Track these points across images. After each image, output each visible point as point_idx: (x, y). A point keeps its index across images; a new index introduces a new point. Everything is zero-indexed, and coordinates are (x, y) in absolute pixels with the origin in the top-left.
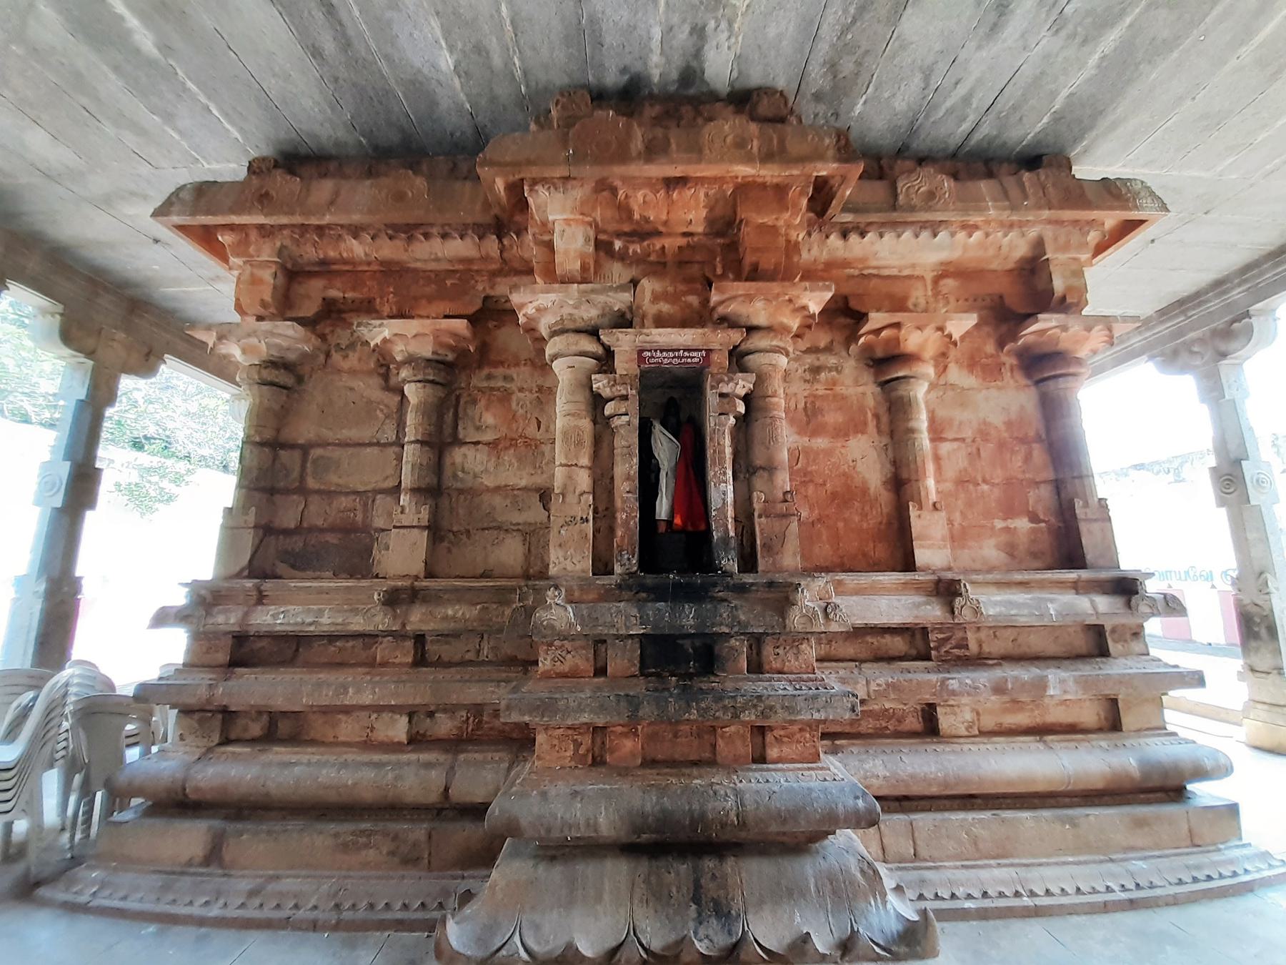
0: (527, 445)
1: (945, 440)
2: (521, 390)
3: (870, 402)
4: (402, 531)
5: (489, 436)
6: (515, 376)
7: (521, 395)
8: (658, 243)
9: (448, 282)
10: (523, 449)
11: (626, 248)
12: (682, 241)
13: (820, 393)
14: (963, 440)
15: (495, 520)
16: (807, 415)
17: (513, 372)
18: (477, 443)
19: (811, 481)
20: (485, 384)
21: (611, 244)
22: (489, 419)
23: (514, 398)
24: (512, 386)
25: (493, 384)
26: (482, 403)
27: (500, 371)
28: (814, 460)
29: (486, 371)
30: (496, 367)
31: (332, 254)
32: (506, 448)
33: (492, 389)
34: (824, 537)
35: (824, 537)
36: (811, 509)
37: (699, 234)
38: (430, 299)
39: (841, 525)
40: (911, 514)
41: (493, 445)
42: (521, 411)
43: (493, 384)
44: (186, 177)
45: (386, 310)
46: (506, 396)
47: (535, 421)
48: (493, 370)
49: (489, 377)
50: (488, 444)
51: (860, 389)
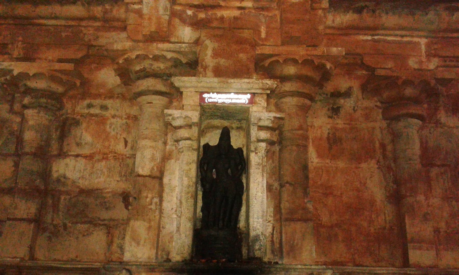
0: (115, 158)
1: (435, 165)
2: (113, 117)
3: (378, 134)
4: (14, 222)
5: (86, 151)
6: (109, 106)
7: (113, 120)
8: (220, 13)
9: (63, 34)
10: (112, 161)
11: (195, 15)
12: (237, 13)
13: (340, 126)
14: (449, 166)
15: (87, 217)
16: (329, 143)
17: (109, 103)
18: (77, 156)
19: (331, 193)
20: (86, 111)
21: (185, 12)
22: (87, 138)
23: (109, 122)
24: (107, 114)
25: (92, 111)
26: (84, 125)
27: (97, 102)
28: (334, 177)
29: (87, 102)
30: (95, 99)
31: (328, 161)
32: (99, 161)
33: (92, 115)
34: (340, 239)
35: (340, 239)
36: (331, 215)
37: (249, 8)
38: (48, 46)
39: (353, 229)
40: (407, 221)
41: (89, 157)
42: (113, 133)
43: (92, 111)
44: (125, 209)
45: (16, 54)
46: (102, 121)
47: (122, 140)
48: (93, 101)
49: (90, 106)
50: (86, 157)
51: (371, 125)
